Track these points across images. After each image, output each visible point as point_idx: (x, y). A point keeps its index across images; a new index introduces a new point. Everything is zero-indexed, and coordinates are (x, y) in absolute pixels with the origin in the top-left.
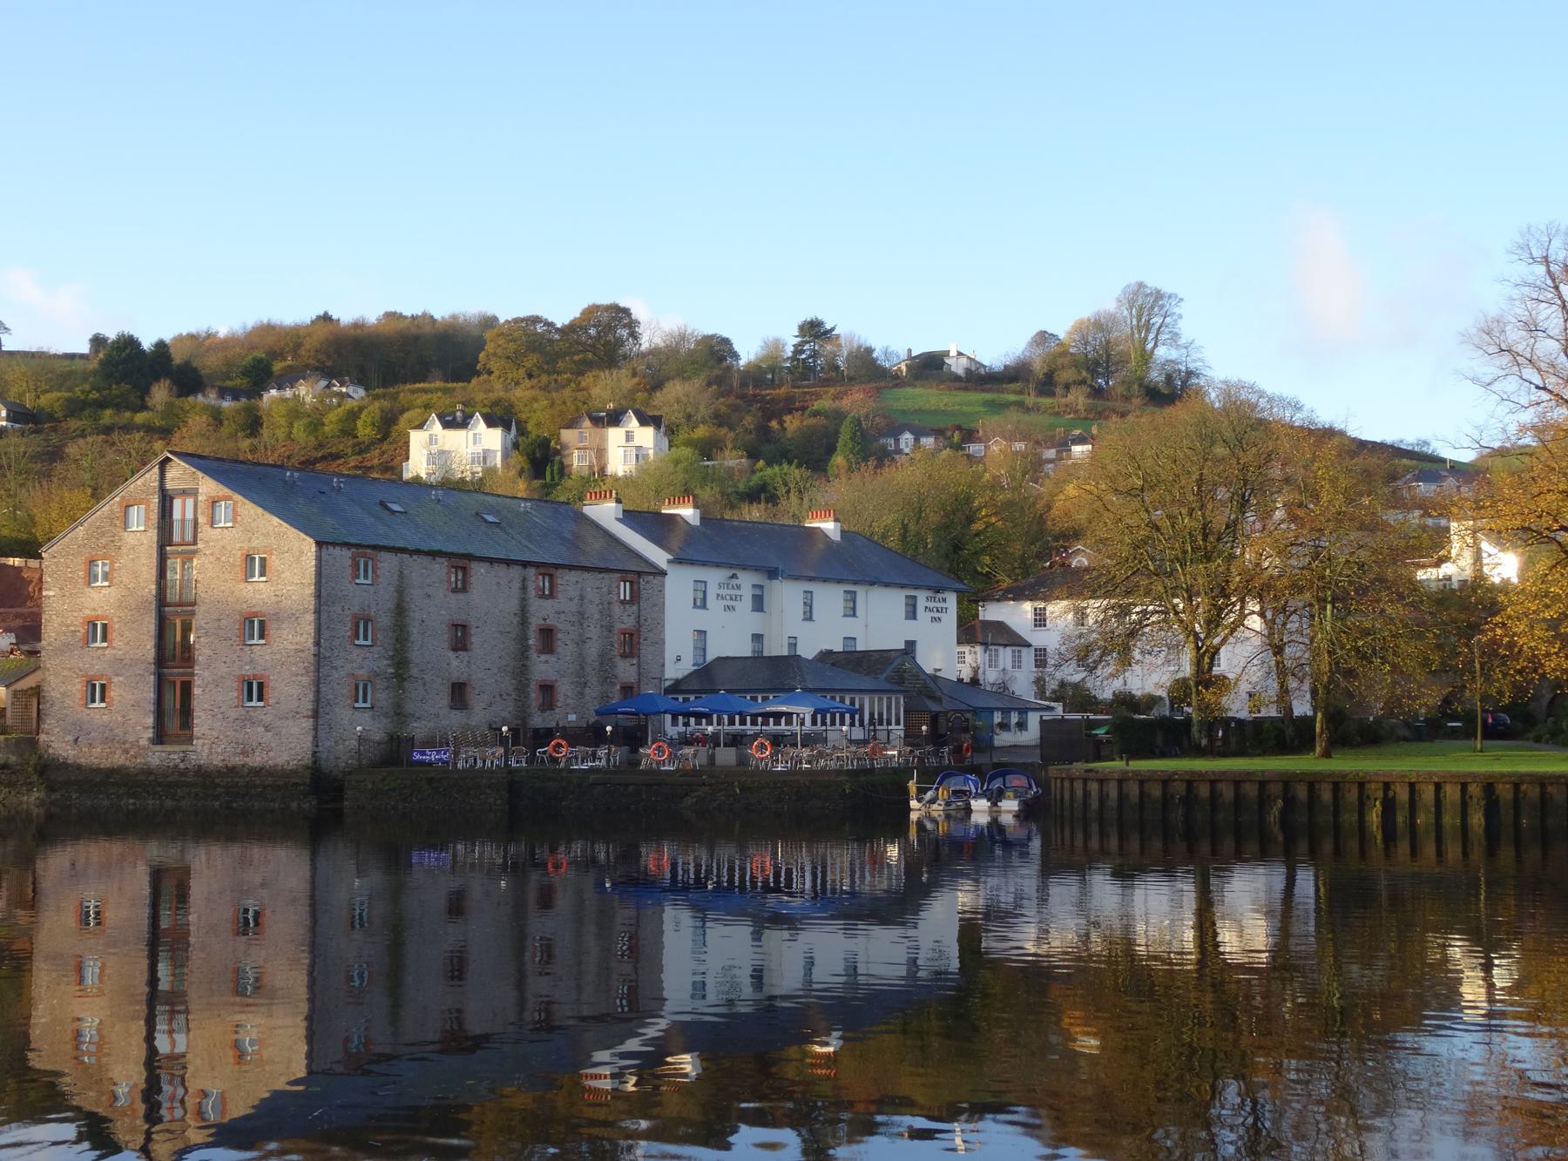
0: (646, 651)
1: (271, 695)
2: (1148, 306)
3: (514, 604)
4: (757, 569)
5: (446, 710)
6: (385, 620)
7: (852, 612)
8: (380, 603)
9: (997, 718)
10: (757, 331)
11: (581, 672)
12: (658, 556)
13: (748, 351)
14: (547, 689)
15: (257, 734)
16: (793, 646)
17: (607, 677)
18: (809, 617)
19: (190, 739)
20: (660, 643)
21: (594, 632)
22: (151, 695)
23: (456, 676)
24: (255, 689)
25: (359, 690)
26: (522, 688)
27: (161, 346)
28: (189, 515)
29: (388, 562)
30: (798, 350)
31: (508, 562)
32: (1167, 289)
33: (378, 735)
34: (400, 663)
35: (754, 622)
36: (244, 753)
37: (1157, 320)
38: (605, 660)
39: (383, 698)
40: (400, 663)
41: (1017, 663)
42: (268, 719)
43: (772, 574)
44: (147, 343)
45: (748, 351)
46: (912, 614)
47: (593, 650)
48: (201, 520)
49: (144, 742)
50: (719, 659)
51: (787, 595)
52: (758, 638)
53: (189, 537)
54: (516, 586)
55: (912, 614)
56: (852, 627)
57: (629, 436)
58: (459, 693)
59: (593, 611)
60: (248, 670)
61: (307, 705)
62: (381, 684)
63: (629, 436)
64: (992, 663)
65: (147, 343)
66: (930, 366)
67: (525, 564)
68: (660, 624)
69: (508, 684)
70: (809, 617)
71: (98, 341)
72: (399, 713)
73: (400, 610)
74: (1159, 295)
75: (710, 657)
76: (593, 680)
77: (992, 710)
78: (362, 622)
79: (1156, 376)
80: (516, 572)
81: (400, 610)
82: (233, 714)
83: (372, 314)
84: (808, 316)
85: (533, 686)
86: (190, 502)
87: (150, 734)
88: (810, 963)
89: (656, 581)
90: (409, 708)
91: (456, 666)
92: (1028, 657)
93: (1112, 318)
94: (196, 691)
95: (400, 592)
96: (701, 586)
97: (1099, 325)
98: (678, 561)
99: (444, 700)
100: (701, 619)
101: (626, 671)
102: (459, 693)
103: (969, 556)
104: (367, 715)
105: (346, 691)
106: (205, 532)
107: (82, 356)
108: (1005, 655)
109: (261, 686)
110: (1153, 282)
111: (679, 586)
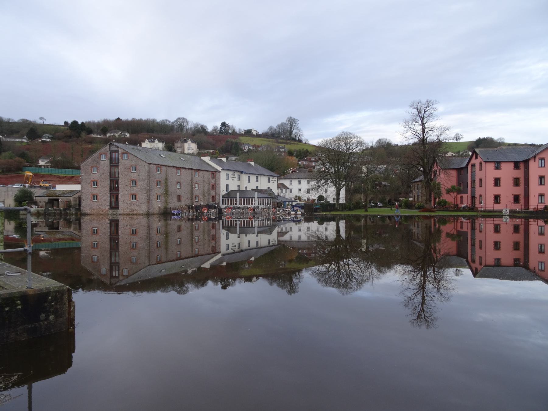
0: (217, 189)
1: (138, 198)
2: (292, 122)
3: (190, 178)
4: (239, 171)
5: (176, 202)
6: (163, 181)
7: (257, 181)
8: (162, 177)
9: (287, 203)
10: (212, 124)
11: (204, 194)
12: (219, 168)
13: (210, 129)
14: (197, 197)
15: (134, 207)
16: (246, 188)
17: (209, 194)
18: (249, 181)
19: (118, 208)
20: (220, 187)
21: (206, 184)
22: (109, 198)
23: (178, 194)
24: (134, 196)
25: (158, 197)
26: (192, 196)
27: (83, 123)
28: (117, 157)
29: (164, 168)
30: (221, 128)
31: (189, 169)
32: (296, 118)
33: (162, 207)
34: (167, 191)
35: (238, 183)
36: (132, 211)
37: (294, 124)
38: (208, 190)
39: (163, 198)
40: (167, 191)
41: (286, 192)
42: (137, 204)
43: (242, 172)
44: (80, 122)
45: (210, 129)
46: (269, 181)
47: (206, 188)
48: (120, 158)
49: (107, 209)
50: (231, 191)
51: (245, 177)
52: (239, 186)
53: (117, 162)
54: (190, 174)
55: (269, 181)
56: (257, 184)
57: (189, 145)
58: (179, 198)
59: (206, 180)
60: (132, 192)
61: (146, 201)
62: (163, 196)
63: (189, 145)
64: (282, 192)
65: (80, 122)
66: (248, 133)
67: (192, 169)
68: (219, 183)
69: (189, 196)
70: (249, 181)
71: (66, 123)
72: (166, 202)
73: (166, 179)
74: (294, 119)
75: (229, 190)
76: (206, 195)
77: (286, 202)
78: (158, 182)
79: (293, 136)
80: (190, 171)
81: (166, 179)
82: (129, 202)
83: (130, 119)
84: (223, 122)
85: (58, 198)
86: (117, 154)
87: (109, 207)
88: (249, 242)
89: (218, 173)
90: (169, 201)
91: (497, 191)
92: (288, 190)
93: (285, 124)
94: (120, 197)
95: (166, 175)
96: (228, 174)
97: (282, 125)
98: (223, 169)
99: (176, 199)
100: (228, 182)
101: (213, 193)
102: (179, 198)
103: (276, 168)
104: (160, 203)
105: (155, 197)
106: (120, 161)
107: (62, 126)
108: (284, 190)
109: (96, 196)
110: (293, 117)
111: (223, 175)
